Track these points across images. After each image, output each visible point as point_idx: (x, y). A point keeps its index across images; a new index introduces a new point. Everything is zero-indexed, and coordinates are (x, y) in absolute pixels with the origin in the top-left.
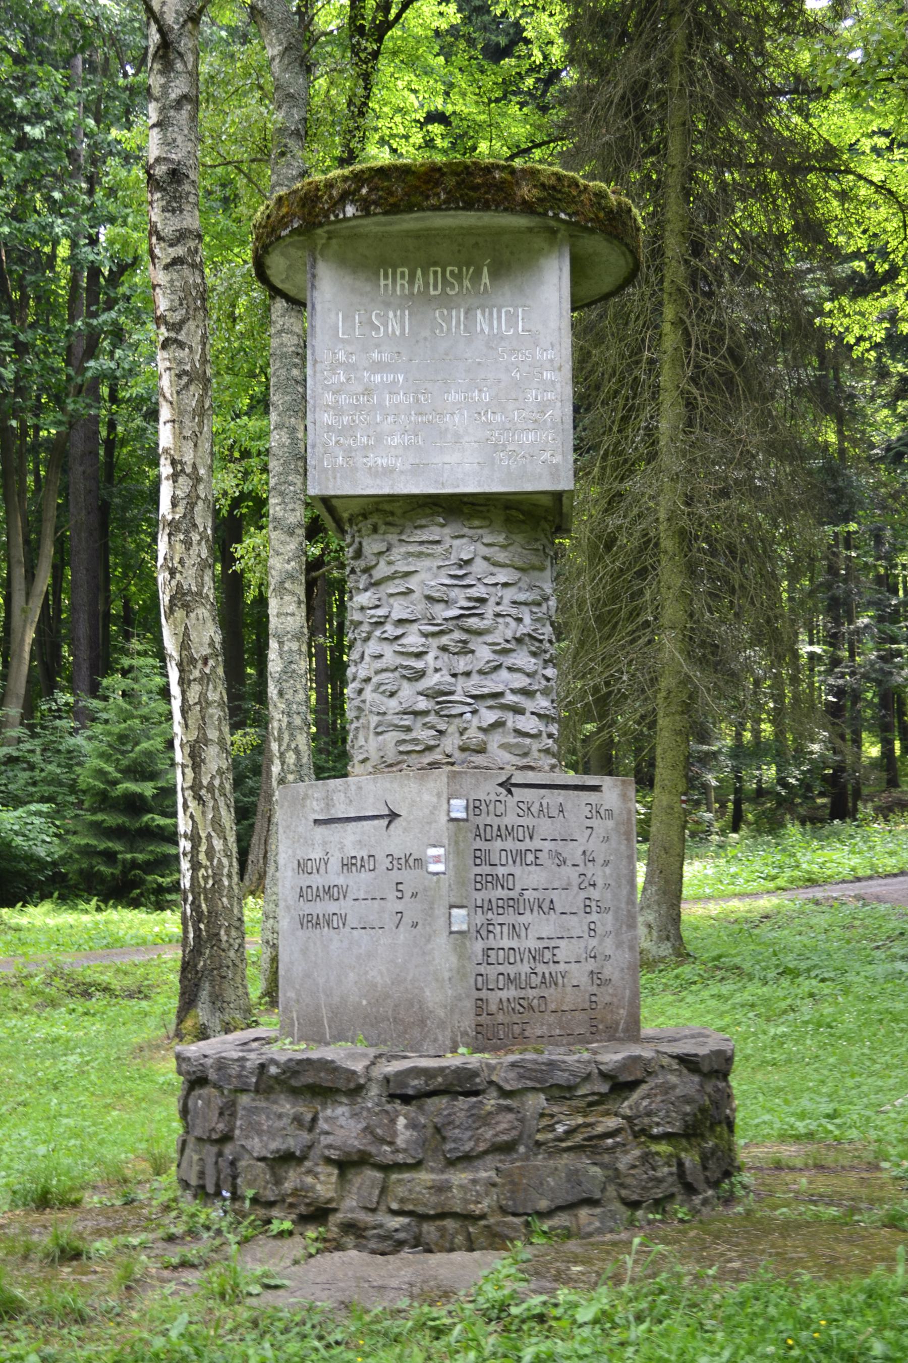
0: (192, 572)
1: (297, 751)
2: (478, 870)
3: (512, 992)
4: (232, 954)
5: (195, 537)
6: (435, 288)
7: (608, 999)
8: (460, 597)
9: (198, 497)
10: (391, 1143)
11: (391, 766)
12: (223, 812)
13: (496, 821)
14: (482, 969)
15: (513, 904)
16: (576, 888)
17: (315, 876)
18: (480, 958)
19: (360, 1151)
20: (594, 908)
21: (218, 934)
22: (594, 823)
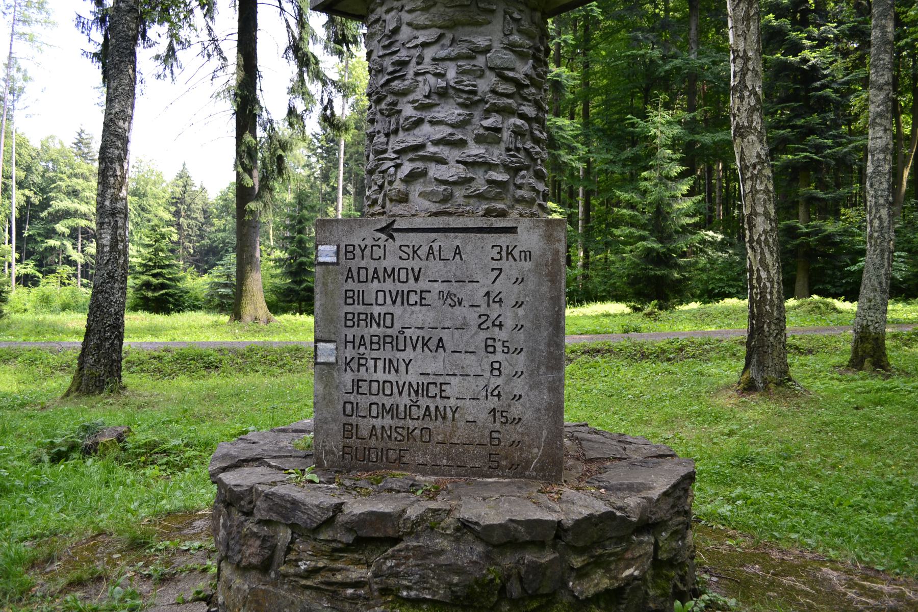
0: (745, 114)
1: (880, 219)
2: (350, 309)
3: (388, 421)
4: (771, 339)
5: (746, 94)
7: (516, 437)
9: (748, 69)
12: (768, 255)
13: (372, 265)
14: (352, 398)
16: (474, 329)
21: (763, 327)
22: (505, 264)
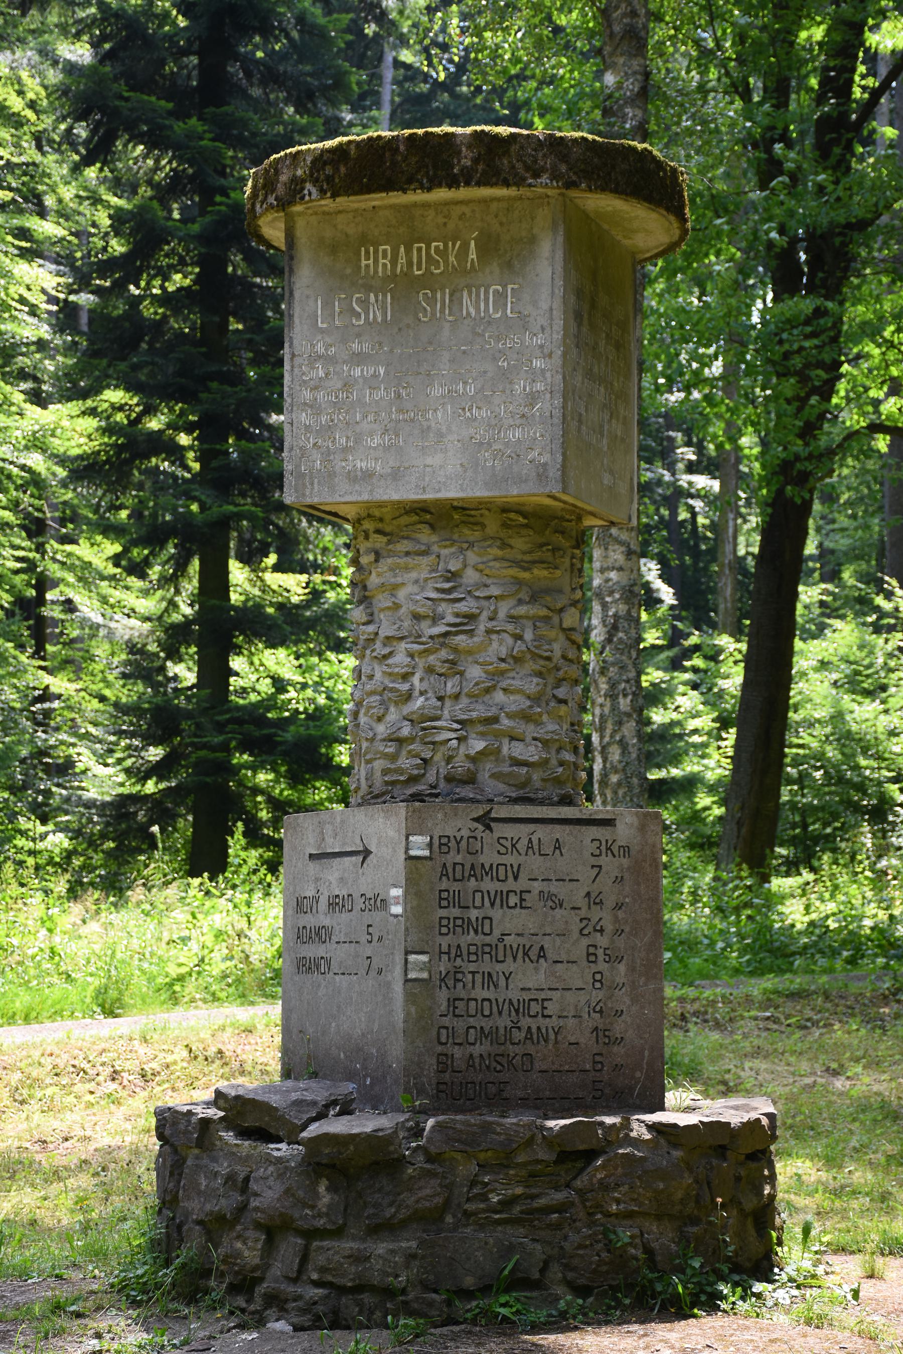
2: (443, 913)
6: (419, 269)
8: (449, 612)
10: (313, 1207)
11: (377, 797)
15: (490, 951)
16: (576, 935)
17: (309, 915)
18: (444, 1007)
19: (281, 1215)
20: (601, 957)
22: (604, 860)
